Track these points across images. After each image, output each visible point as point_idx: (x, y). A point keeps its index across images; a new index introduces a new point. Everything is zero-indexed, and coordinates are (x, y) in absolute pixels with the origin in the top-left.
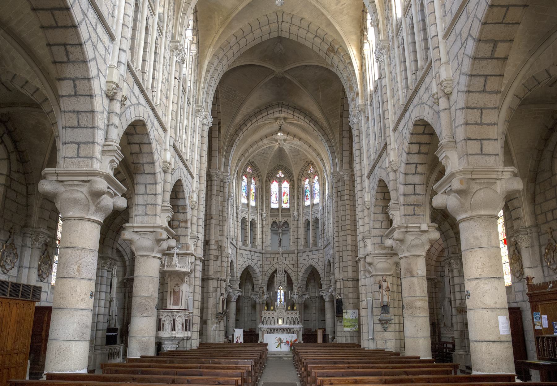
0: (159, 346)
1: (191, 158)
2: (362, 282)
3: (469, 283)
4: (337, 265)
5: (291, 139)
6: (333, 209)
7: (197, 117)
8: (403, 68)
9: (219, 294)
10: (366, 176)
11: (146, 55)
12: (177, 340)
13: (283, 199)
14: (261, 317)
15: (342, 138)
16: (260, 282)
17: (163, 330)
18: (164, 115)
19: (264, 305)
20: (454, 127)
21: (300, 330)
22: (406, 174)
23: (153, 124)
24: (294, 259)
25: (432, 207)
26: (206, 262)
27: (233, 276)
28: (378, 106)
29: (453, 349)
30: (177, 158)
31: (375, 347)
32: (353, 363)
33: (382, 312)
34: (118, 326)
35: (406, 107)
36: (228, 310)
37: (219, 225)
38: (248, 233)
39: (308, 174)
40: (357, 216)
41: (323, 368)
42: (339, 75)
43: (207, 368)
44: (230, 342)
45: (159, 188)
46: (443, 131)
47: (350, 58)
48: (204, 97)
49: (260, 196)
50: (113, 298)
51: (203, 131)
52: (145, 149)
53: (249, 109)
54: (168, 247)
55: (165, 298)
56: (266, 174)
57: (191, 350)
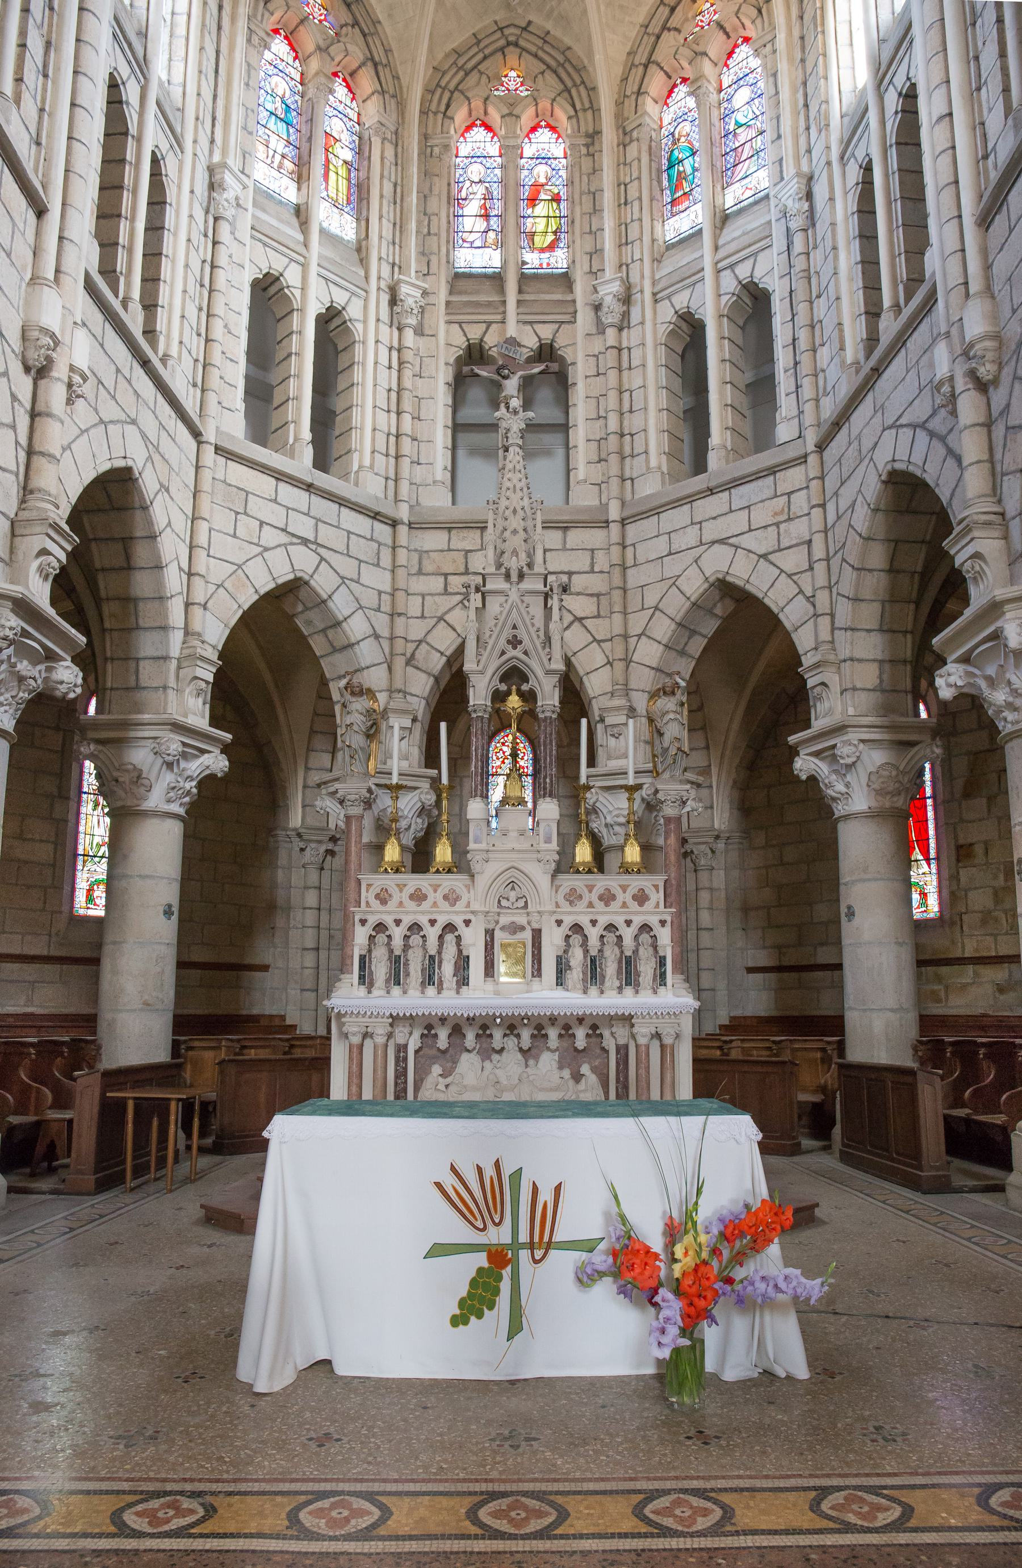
24: (602, 562)
49: (388, 188)
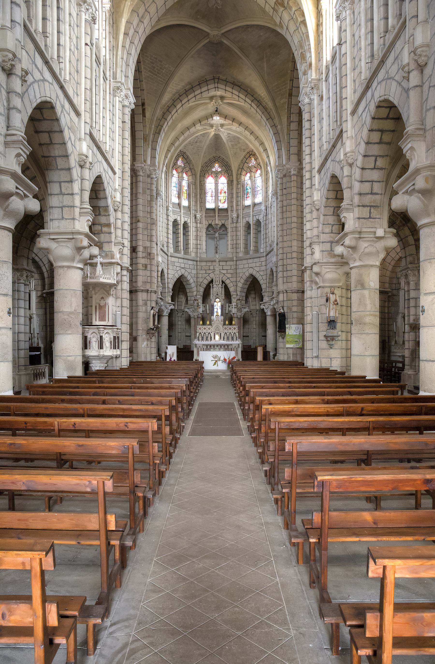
0: (86, 365)
1: (111, 149)
2: (308, 294)
3: (425, 297)
4: (280, 274)
5: (229, 124)
6: (277, 210)
7: (115, 96)
8: (369, 41)
9: (149, 308)
10: (316, 171)
11: (46, 10)
12: (106, 358)
13: (220, 198)
14: (196, 332)
15: (289, 122)
16: (195, 293)
17: (90, 349)
18: (75, 95)
19: (199, 319)
20: (424, 110)
21: (239, 347)
22: (363, 169)
23: (63, 107)
24: (233, 268)
25: (391, 209)
26: (133, 272)
27: (164, 288)
28: (334, 82)
29: (403, 369)
30: (95, 149)
31: (319, 365)
32: (294, 382)
33: (329, 328)
34: (41, 345)
35: (368, 83)
36: (159, 326)
37: (147, 229)
38: (180, 237)
39: (249, 167)
40: (304, 218)
41: (262, 388)
42: (289, 39)
43: (139, 388)
44: (163, 360)
45: (76, 187)
46: (411, 115)
47: (303, 15)
48: (124, 70)
49: (194, 194)
50: (33, 314)
51: (123, 114)
52: (56, 138)
53: (179, 85)
54: (90, 256)
55: (90, 313)
56: (200, 168)
57: (121, 369)
